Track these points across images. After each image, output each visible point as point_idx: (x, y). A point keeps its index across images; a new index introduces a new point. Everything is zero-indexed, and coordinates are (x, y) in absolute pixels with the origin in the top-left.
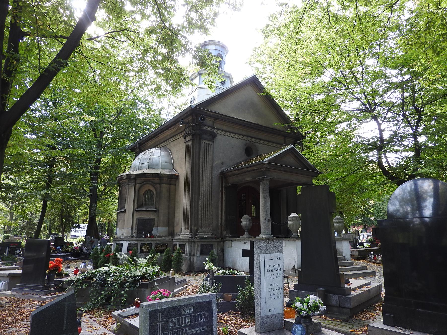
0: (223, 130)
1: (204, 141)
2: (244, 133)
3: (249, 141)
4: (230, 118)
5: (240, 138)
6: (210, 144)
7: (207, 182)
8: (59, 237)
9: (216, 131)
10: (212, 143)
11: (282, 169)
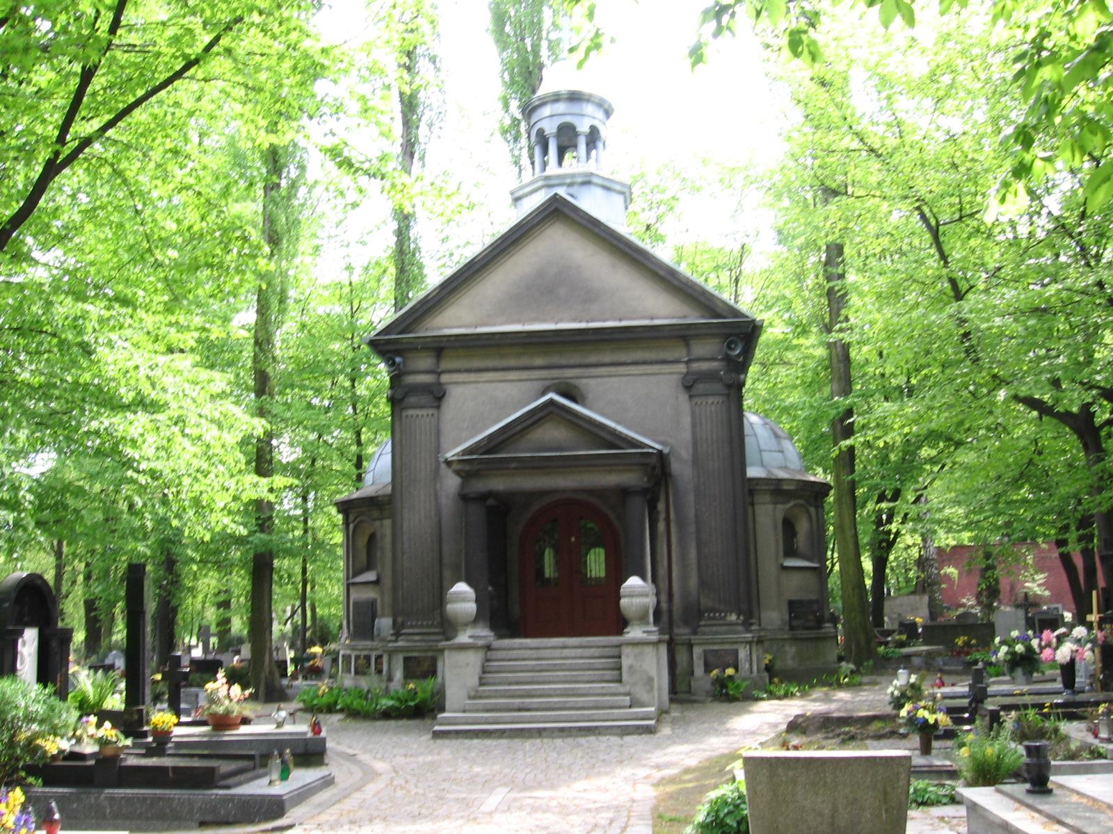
0: (468, 371)
1: (411, 412)
3: (553, 379)
5: (524, 377)
9: (445, 378)
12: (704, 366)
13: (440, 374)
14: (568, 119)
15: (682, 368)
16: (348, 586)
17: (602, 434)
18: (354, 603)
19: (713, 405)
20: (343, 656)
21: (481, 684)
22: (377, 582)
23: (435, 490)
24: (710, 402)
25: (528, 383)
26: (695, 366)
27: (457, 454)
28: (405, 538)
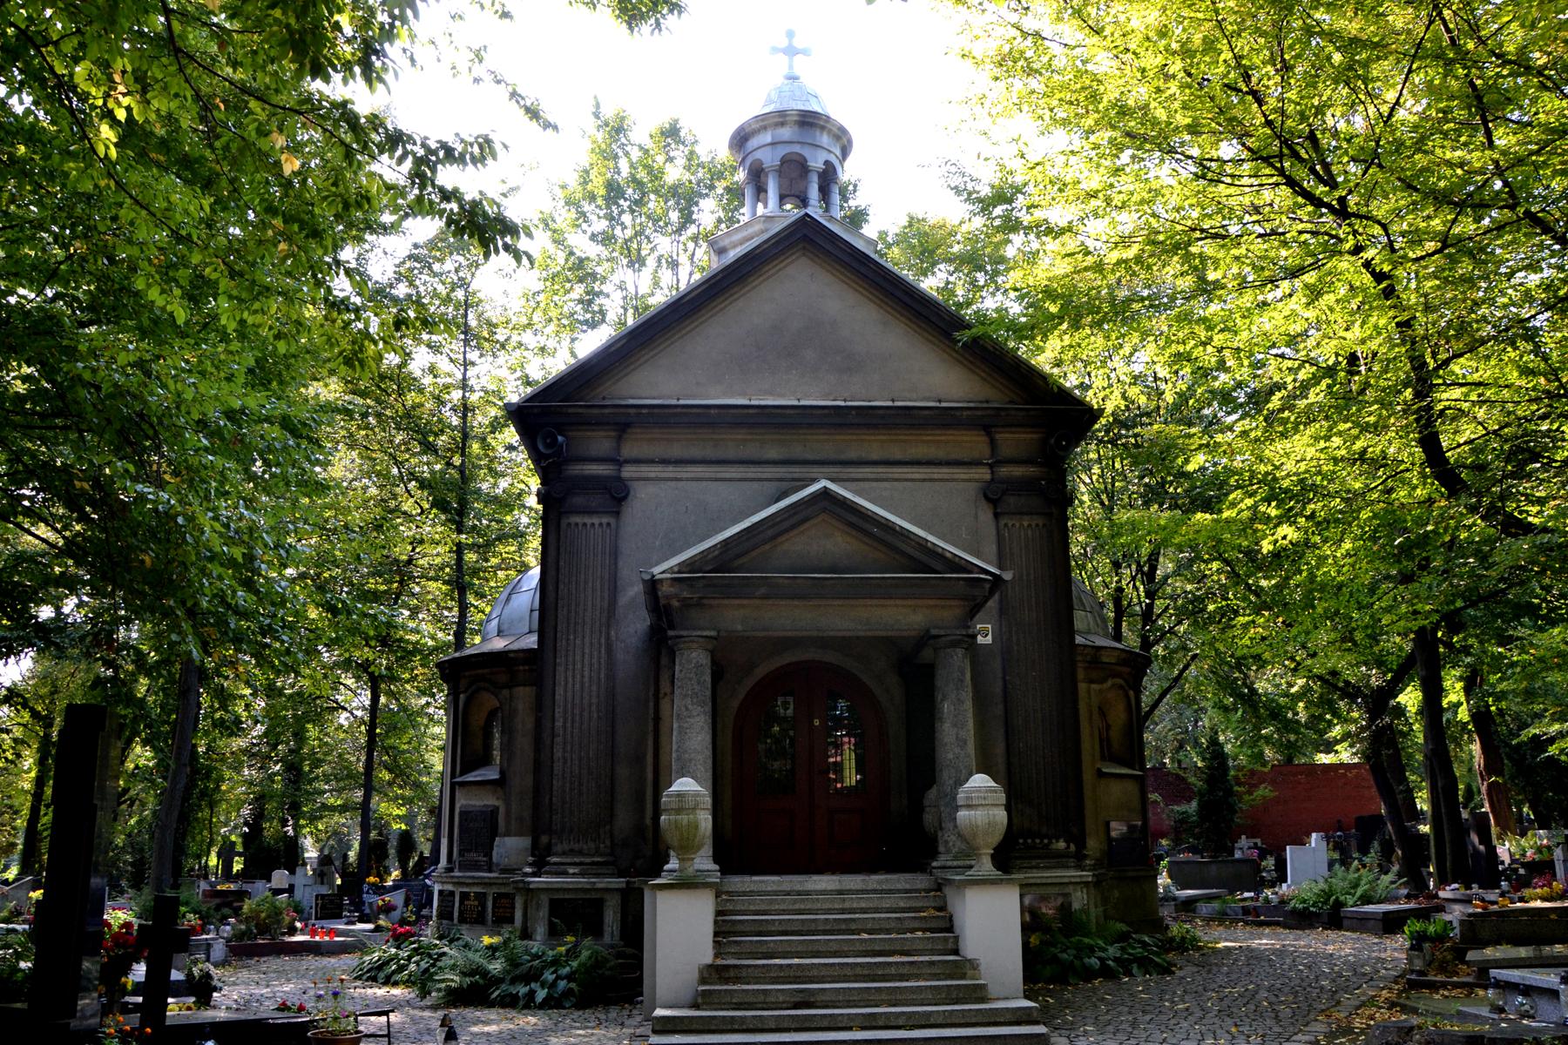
0: (665, 462)
2: (773, 453)
4: (679, 410)
5: (750, 475)
6: (601, 524)
7: (587, 669)
8: (847, 783)
9: (628, 472)
10: (612, 521)
11: (763, 590)
12: (1017, 471)
13: (620, 463)
14: (797, 149)
15: (984, 474)
16: (453, 786)
17: (903, 547)
18: (461, 813)
19: (1025, 527)
20: (441, 892)
21: (716, 956)
22: (500, 784)
23: (608, 638)
24: (1026, 524)
25: (755, 485)
26: (1004, 471)
27: (670, 570)
28: (559, 711)
